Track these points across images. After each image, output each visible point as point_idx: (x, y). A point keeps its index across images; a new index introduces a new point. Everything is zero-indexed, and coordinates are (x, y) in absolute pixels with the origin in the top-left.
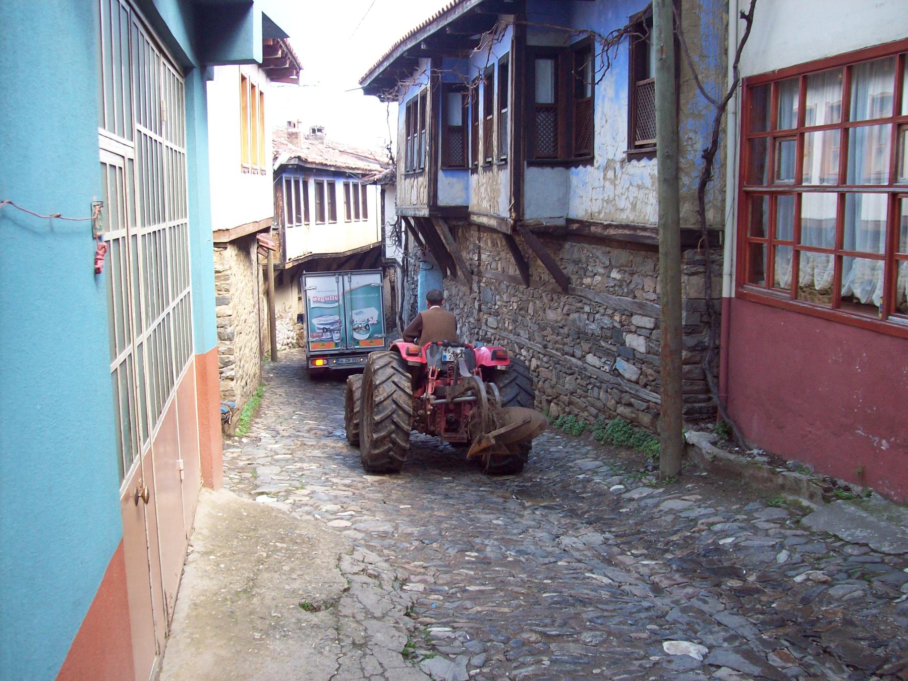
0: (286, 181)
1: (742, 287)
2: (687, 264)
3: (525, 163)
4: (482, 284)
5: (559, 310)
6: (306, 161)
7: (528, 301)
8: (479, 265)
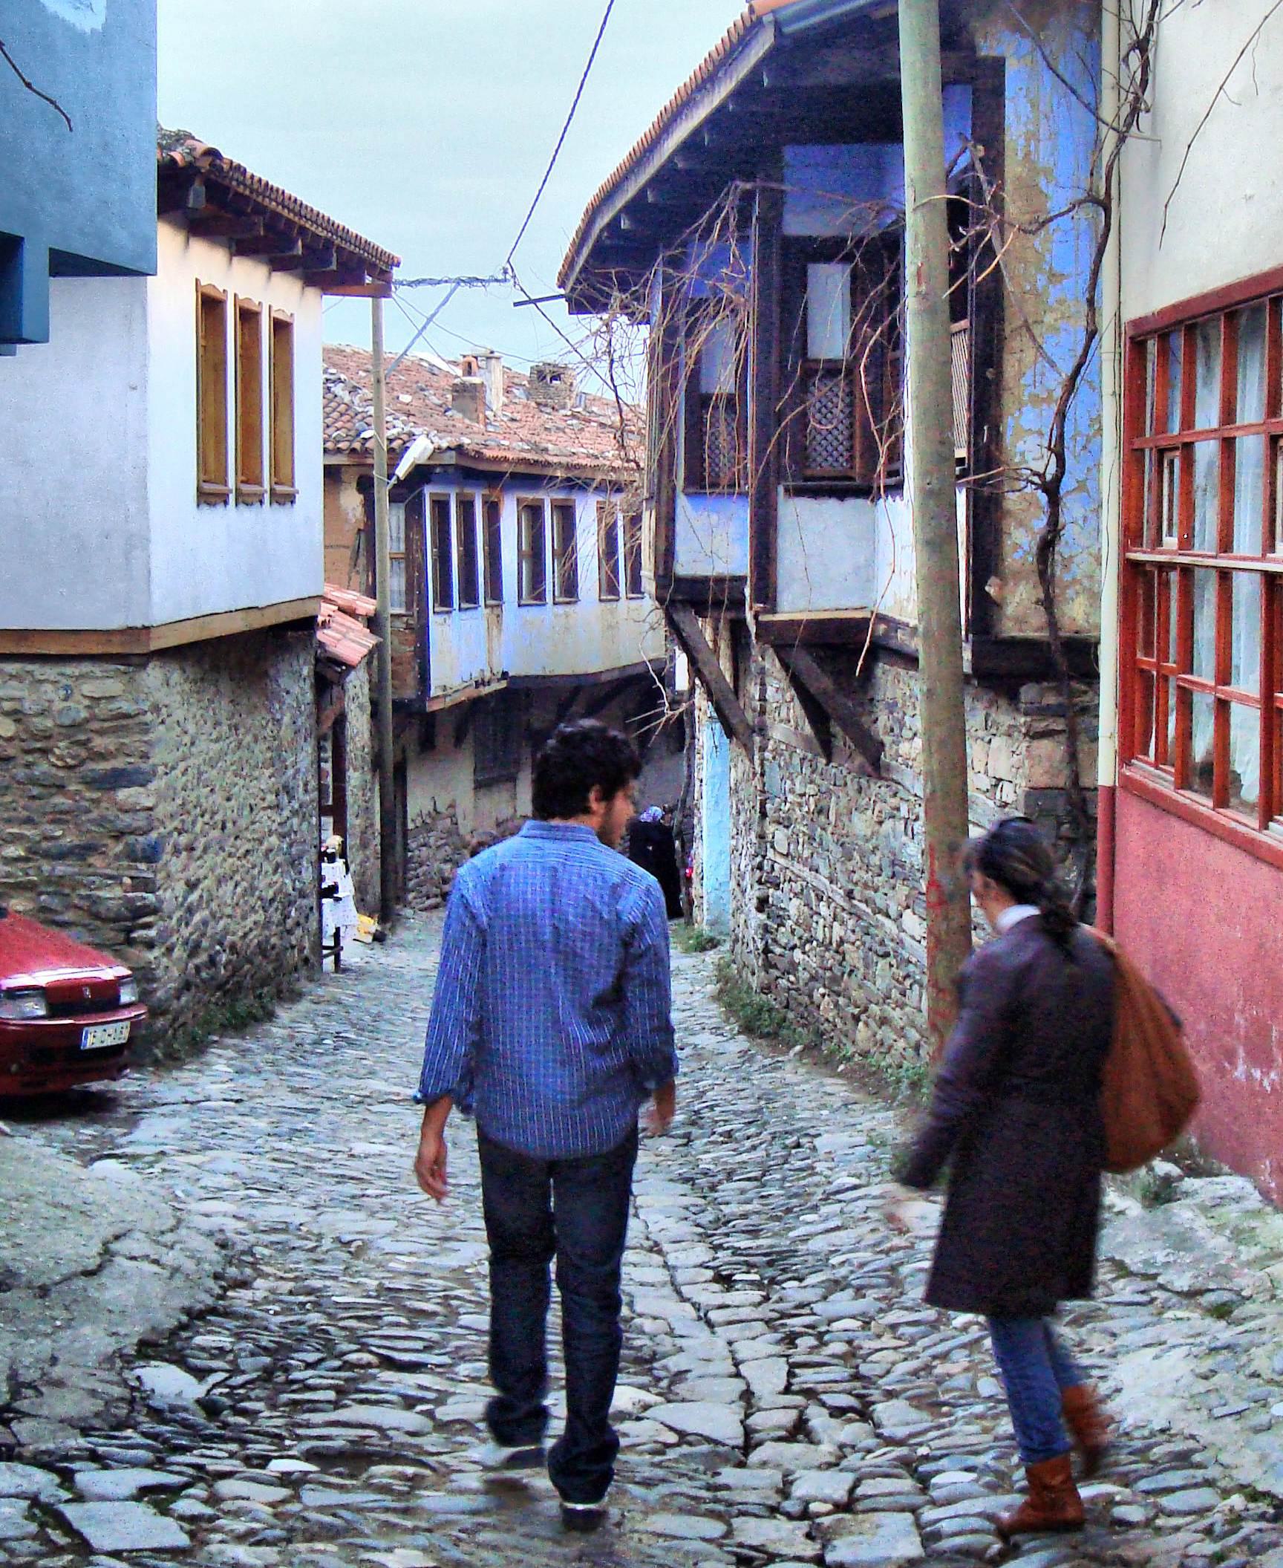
0: (434, 502)
1: (1129, 764)
2: (1026, 714)
3: (781, 489)
4: (768, 755)
5: (869, 812)
6: (479, 456)
7: (829, 792)
8: (763, 712)
